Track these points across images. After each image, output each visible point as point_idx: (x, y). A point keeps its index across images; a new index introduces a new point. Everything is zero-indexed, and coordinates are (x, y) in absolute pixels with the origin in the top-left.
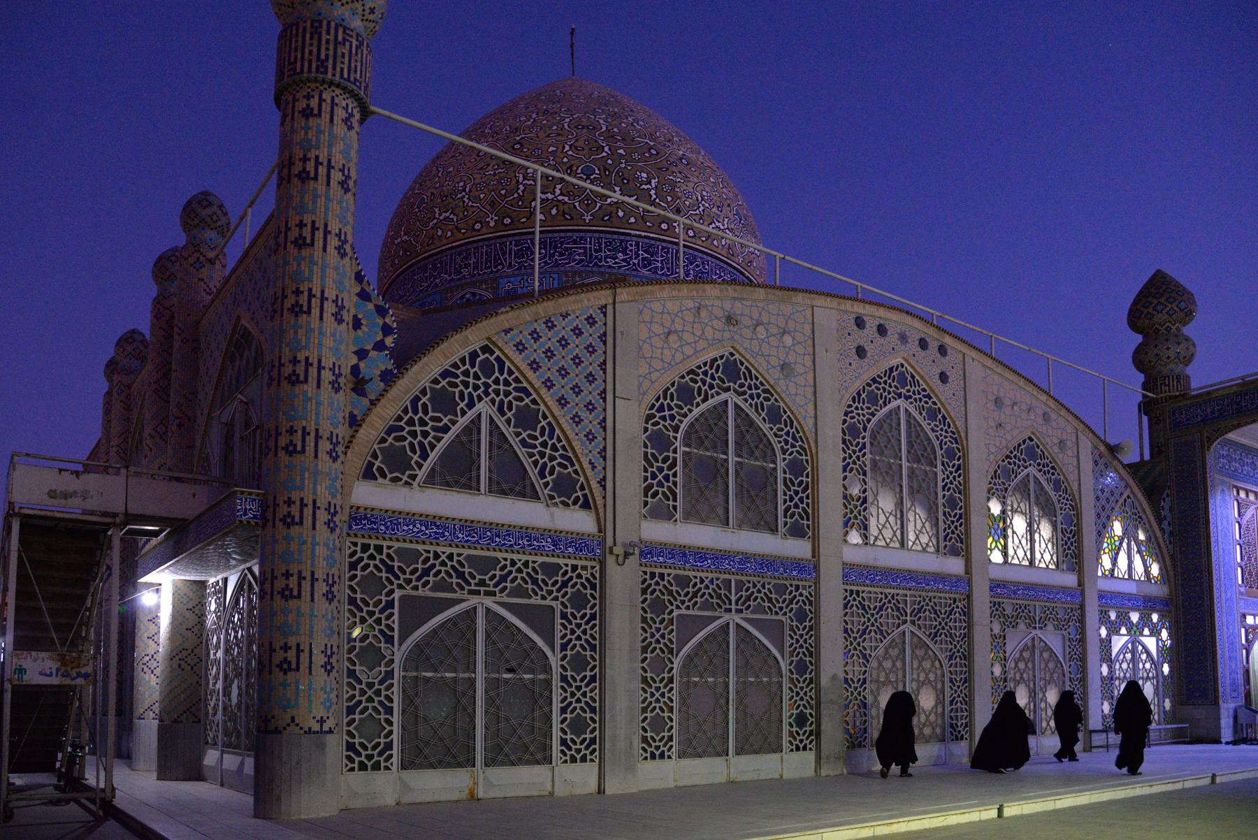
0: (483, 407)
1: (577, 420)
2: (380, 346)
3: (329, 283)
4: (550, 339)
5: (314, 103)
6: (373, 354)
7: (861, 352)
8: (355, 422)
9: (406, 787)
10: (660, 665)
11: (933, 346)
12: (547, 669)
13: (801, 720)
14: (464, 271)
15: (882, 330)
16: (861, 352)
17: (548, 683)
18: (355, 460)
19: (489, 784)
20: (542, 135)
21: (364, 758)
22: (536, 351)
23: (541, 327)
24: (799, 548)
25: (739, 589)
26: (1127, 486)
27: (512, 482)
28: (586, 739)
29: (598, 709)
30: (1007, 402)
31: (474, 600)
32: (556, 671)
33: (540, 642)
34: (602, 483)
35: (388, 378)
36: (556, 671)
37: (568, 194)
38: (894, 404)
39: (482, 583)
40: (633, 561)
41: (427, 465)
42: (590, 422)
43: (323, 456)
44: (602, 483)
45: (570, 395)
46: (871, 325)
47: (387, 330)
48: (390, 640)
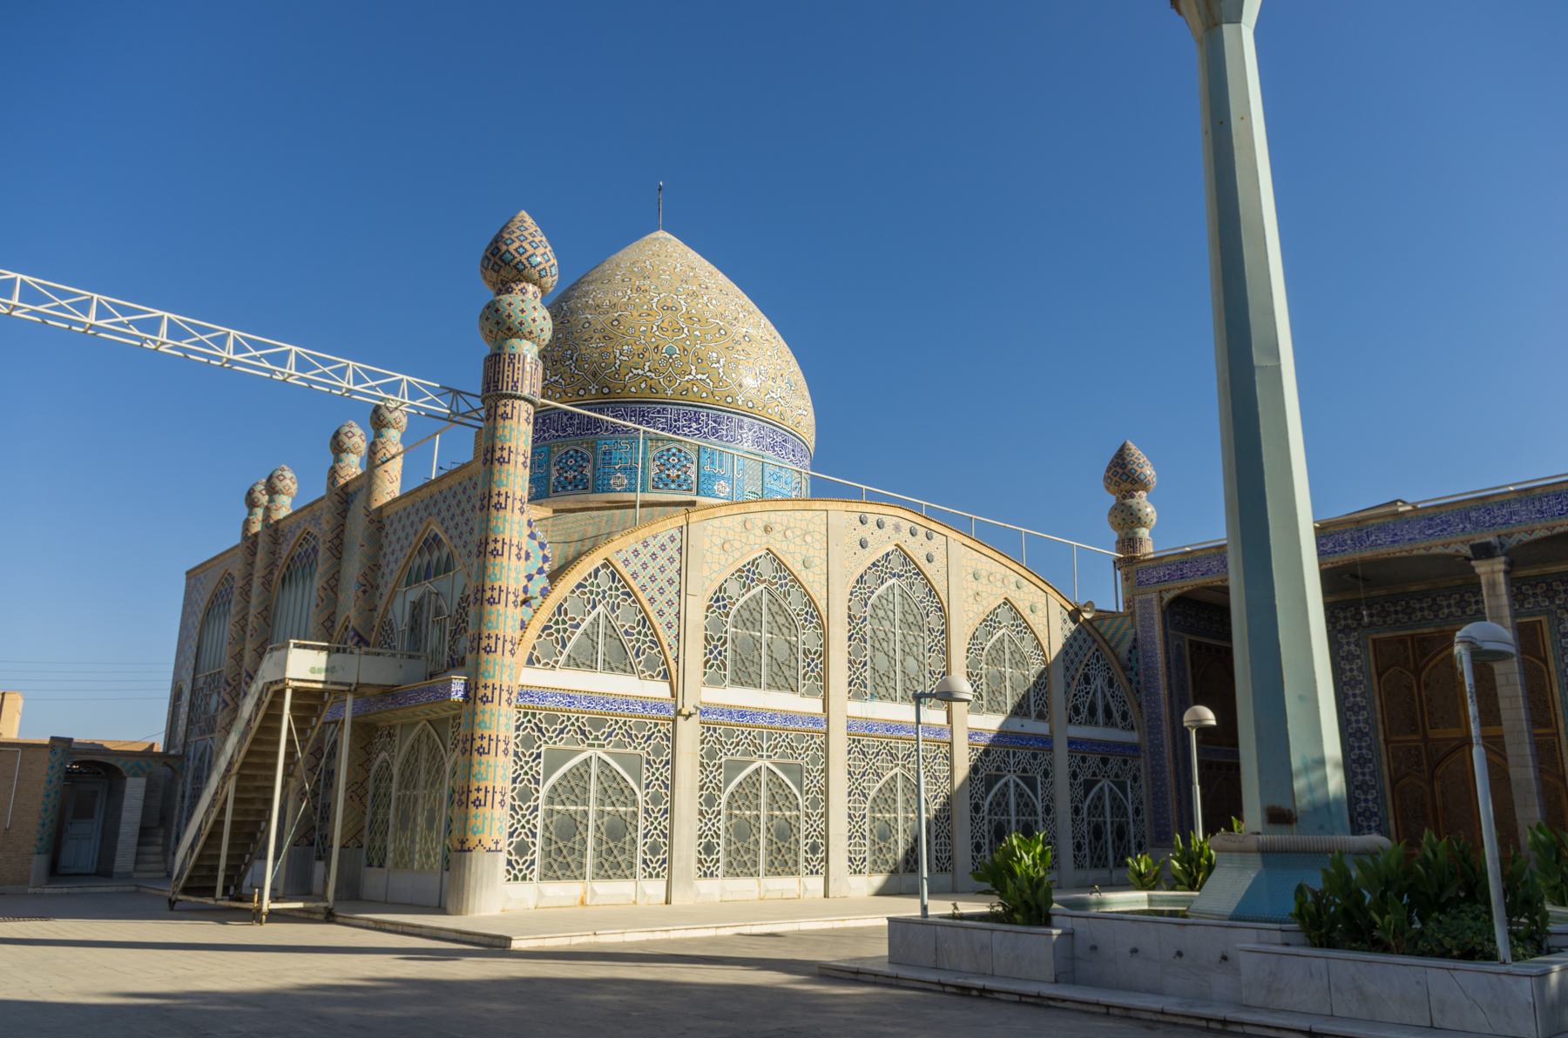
0: (600, 608)
1: (661, 613)
2: (540, 571)
3: (515, 534)
4: (645, 556)
5: (509, 409)
6: (536, 577)
7: (863, 545)
8: (524, 626)
9: (541, 895)
10: (710, 801)
11: (921, 532)
12: (635, 803)
13: (814, 849)
14: (569, 430)
15: (880, 525)
16: (863, 545)
17: (635, 814)
18: (523, 653)
19: (594, 893)
20: (636, 314)
21: (517, 874)
22: (635, 565)
23: (640, 547)
24: (813, 705)
25: (769, 739)
26: (1094, 641)
27: (620, 662)
28: (660, 860)
29: (668, 835)
30: (984, 573)
31: (590, 752)
32: (642, 805)
33: (632, 783)
34: (676, 660)
35: (545, 593)
36: (642, 805)
37: (655, 371)
38: (890, 582)
39: (597, 738)
40: (695, 719)
41: (566, 652)
42: (670, 613)
43: (507, 653)
44: (676, 660)
45: (657, 595)
46: (872, 519)
47: (545, 559)
48: (537, 782)
